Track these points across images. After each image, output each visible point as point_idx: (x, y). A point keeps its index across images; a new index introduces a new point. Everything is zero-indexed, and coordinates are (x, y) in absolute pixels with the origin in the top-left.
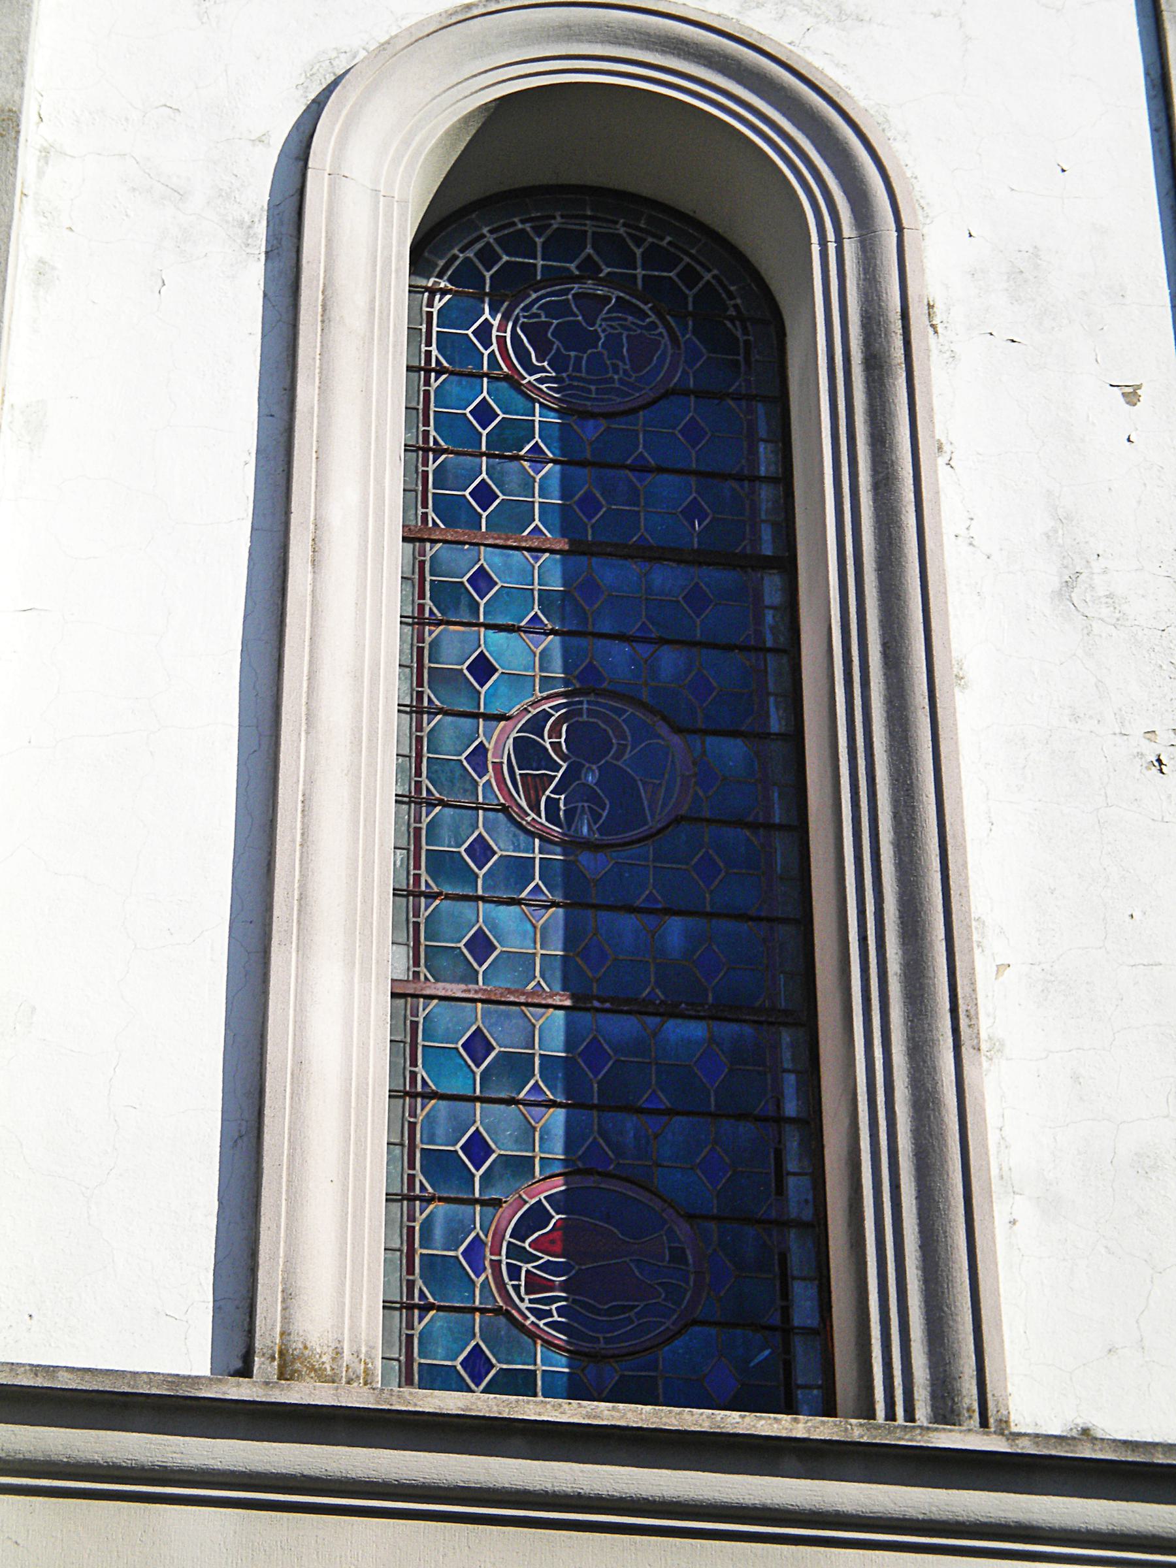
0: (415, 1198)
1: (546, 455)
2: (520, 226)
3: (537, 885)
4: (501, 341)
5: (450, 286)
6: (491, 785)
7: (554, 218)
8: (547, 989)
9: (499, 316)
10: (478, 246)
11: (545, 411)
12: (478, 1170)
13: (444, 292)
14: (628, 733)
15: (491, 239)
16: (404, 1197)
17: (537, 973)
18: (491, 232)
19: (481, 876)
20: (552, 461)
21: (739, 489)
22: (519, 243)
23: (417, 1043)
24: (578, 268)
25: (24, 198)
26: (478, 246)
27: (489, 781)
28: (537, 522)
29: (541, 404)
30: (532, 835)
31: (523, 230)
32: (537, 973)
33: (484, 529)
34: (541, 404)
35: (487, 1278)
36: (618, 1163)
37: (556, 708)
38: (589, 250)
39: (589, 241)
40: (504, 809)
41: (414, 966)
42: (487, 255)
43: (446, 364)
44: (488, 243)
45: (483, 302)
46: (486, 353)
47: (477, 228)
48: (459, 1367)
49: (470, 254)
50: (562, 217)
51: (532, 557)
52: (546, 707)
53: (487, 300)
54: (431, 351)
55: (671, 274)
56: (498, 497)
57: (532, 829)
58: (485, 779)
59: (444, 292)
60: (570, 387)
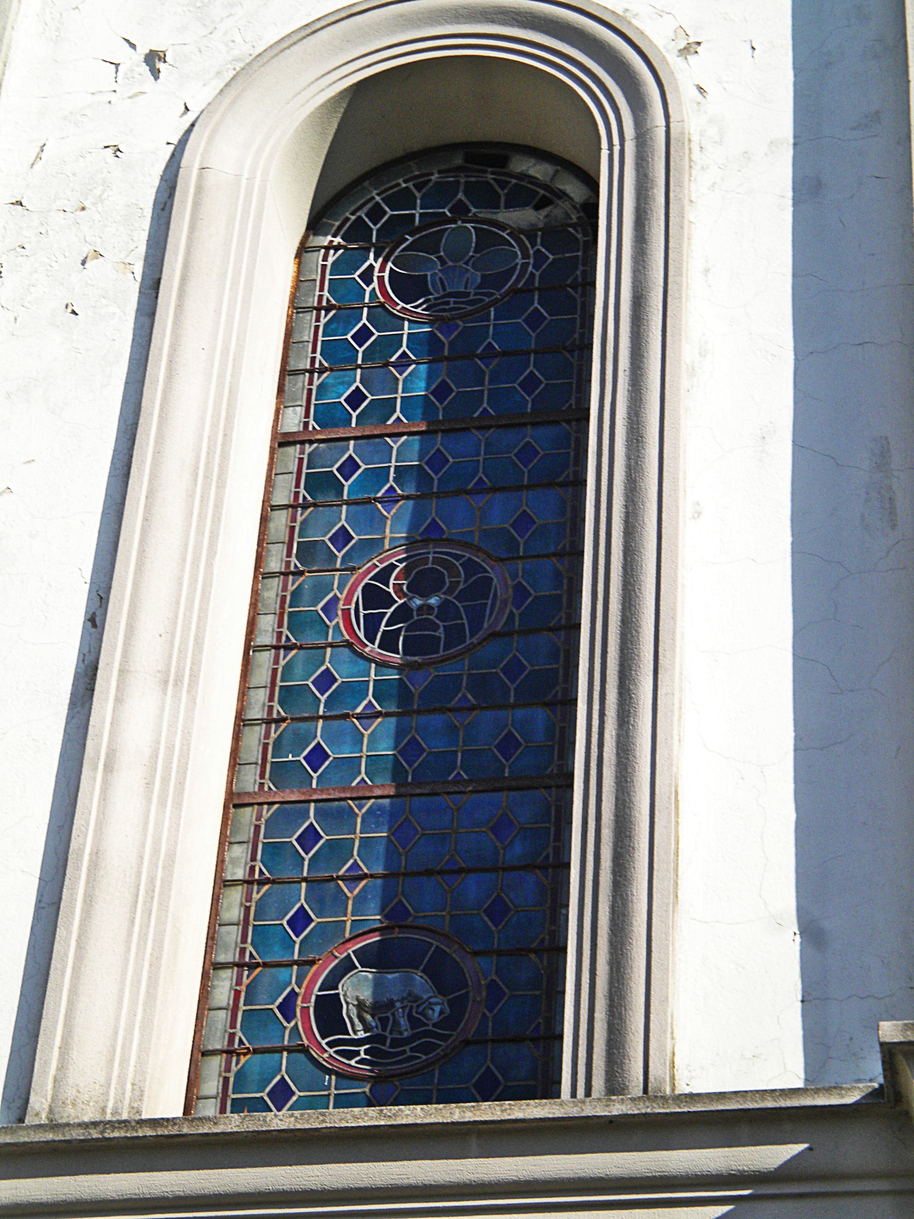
0: (246, 965)
1: (410, 358)
2: (404, 185)
3: (398, 418)
4: (381, 279)
5: (343, 243)
6: (339, 628)
7: (432, 174)
8: (369, 783)
9: (380, 260)
10: (369, 206)
11: (412, 325)
12: (307, 853)
13: (337, 248)
14: (462, 572)
15: (378, 198)
16: (227, 1052)
17: (355, 853)
18: (378, 194)
19: (332, 627)
20: (403, 498)
21: (547, 796)
22: (402, 199)
23: (258, 840)
24: (450, 211)
25: (38, 159)
26: (369, 206)
27: (374, 289)
28: (363, 775)
29: (409, 320)
30: (370, 661)
31: (407, 188)
32: (355, 853)
33: (353, 425)
34: (409, 320)
35: (296, 1024)
36: (402, 1090)
37: (400, 561)
38: (460, 196)
39: (462, 188)
40: (349, 645)
41: (261, 779)
42: (376, 213)
43: (334, 302)
44: (377, 203)
45: (369, 252)
46: (368, 290)
47: (370, 192)
48: (266, 1098)
49: (362, 213)
50: (439, 172)
51: (392, 441)
52: (393, 561)
53: (373, 250)
54: (272, 706)
55: (519, 321)
56: (367, 397)
57: (330, 1067)
58: (371, 287)
59: (337, 248)
60: (435, 305)
